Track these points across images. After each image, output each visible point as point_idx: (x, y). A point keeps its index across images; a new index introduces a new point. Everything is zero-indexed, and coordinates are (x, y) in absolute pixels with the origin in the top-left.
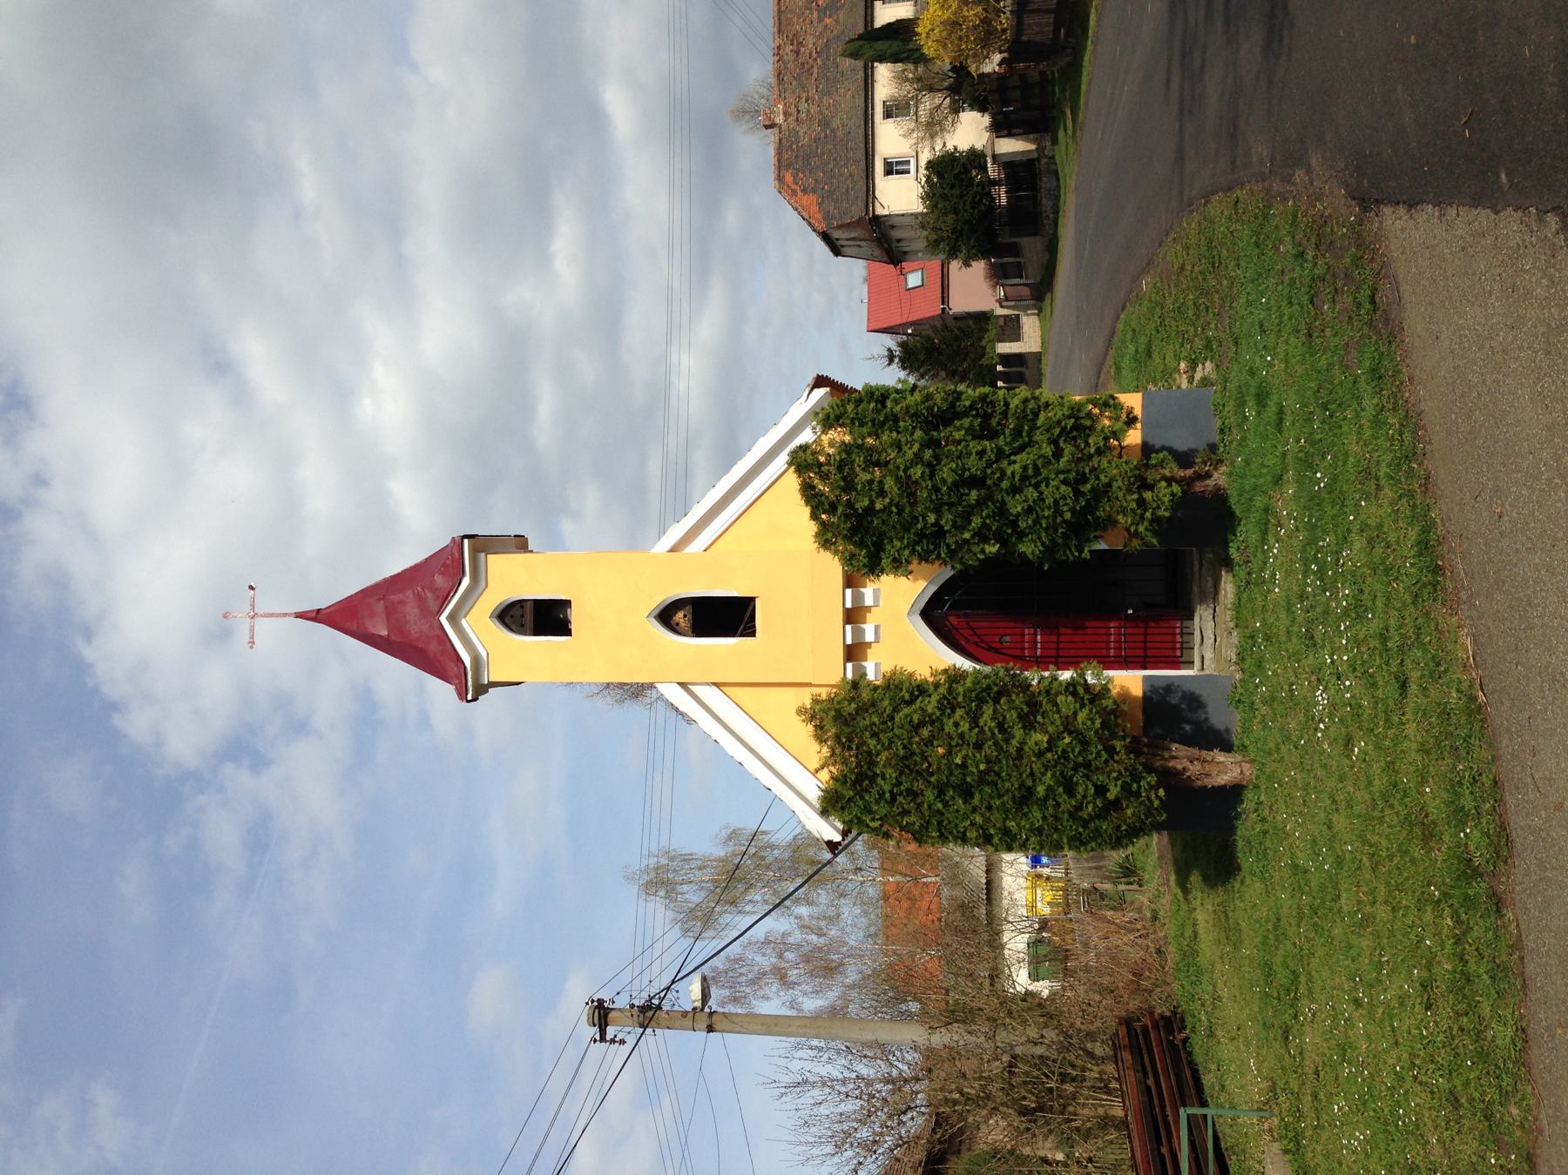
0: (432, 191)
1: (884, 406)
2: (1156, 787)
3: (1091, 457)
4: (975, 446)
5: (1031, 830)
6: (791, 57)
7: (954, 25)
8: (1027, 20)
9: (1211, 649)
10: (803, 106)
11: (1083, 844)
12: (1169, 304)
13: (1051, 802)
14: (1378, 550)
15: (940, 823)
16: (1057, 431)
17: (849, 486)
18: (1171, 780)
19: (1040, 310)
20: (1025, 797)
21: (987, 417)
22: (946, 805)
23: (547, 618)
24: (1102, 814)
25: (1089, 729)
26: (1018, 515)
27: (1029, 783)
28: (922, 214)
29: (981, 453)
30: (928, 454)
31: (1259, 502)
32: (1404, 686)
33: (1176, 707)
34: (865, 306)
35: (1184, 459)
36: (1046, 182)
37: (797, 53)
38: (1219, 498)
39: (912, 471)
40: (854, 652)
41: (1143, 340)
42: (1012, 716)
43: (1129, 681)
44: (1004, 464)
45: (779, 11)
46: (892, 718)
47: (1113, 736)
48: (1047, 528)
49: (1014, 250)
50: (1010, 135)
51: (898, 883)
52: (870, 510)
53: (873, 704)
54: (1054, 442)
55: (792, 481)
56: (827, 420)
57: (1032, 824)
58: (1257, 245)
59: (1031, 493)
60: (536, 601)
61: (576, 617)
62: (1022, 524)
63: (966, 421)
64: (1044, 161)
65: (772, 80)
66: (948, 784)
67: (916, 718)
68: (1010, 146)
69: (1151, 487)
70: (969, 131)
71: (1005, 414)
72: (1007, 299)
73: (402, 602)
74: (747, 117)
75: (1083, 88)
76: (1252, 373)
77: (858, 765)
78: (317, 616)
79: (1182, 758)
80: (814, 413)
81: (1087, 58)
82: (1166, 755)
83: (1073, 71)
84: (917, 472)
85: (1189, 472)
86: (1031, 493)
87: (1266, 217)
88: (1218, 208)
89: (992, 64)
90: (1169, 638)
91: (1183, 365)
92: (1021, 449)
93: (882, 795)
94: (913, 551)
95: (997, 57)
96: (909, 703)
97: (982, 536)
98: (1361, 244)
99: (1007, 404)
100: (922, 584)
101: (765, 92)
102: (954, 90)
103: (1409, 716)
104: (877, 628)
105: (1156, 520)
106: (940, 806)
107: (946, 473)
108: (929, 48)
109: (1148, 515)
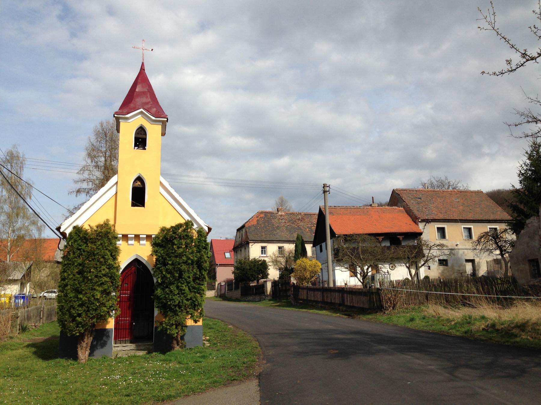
0: (260, 101)
1: (203, 249)
2: (79, 333)
3: (186, 310)
4: (191, 275)
5: (66, 293)
6: (298, 217)
7: (305, 269)
8: (305, 291)
9: (122, 349)
10: (283, 221)
11: (60, 310)
12: (225, 333)
13: (76, 300)
14: (167, 386)
15: (70, 264)
16: (194, 300)
17: (180, 238)
18: (82, 337)
19: (217, 297)
20: (78, 291)
21: (199, 279)
22: (76, 266)
23: (140, 141)
24: (71, 316)
25: (101, 311)
26: (170, 288)
27: (83, 293)
28: (249, 259)
29: (189, 277)
30: (190, 262)
31: (173, 358)
32: (128, 396)
33: (102, 339)
34: (219, 239)
35: (182, 338)
36: (257, 298)
37: (299, 220)
38: (171, 348)
39: (185, 257)
40: (125, 237)
41: (214, 327)
42: (106, 287)
43: (111, 324)
44: (186, 284)
45: (311, 215)
46: (106, 250)
47: (98, 318)
48: (165, 297)
49: (237, 288)
50: (272, 286)
51: (7, 246)
52: (173, 244)
53: (111, 244)
54: (191, 299)
55: (183, 221)
56: (200, 232)
57: (69, 293)
58: (246, 353)
59: (176, 292)
60: (146, 139)
61: (140, 151)
62: (167, 289)
63: (198, 273)
64: (264, 297)
65: (291, 211)
66: (84, 267)
67: (106, 257)
68: (269, 286)
69: (176, 328)
70: (274, 274)
71: (199, 284)
72: (221, 286)
73: (147, 97)
74: (280, 202)
75: (285, 308)
76: (210, 354)
77: (91, 239)
78: (142, 69)
79: (88, 340)
80: (202, 228)
81: (294, 309)
82: (89, 336)
83: (290, 305)
84: (184, 258)
85: (179, 339)
86: (176, 292)
87: (253, 355)
88: (255, 344)
89: (293, 281)
90: (122, 336)
91: (208, 338)
92: (189, 289)
93: (80, 246)
94: (160, 257)
95: (295, 282)
96: (111, 255)
97: (164, 277)
98: (248, 376)
99: (202, 285)
100: (146, 259)
101: (288, 208)
102: (286, 269)
103: (120, 397)
104: (133, 245)
105: (166, 329)
106: (76, 264)
107: (184, 267)
108: (299, 262)
109: (168, 327)
